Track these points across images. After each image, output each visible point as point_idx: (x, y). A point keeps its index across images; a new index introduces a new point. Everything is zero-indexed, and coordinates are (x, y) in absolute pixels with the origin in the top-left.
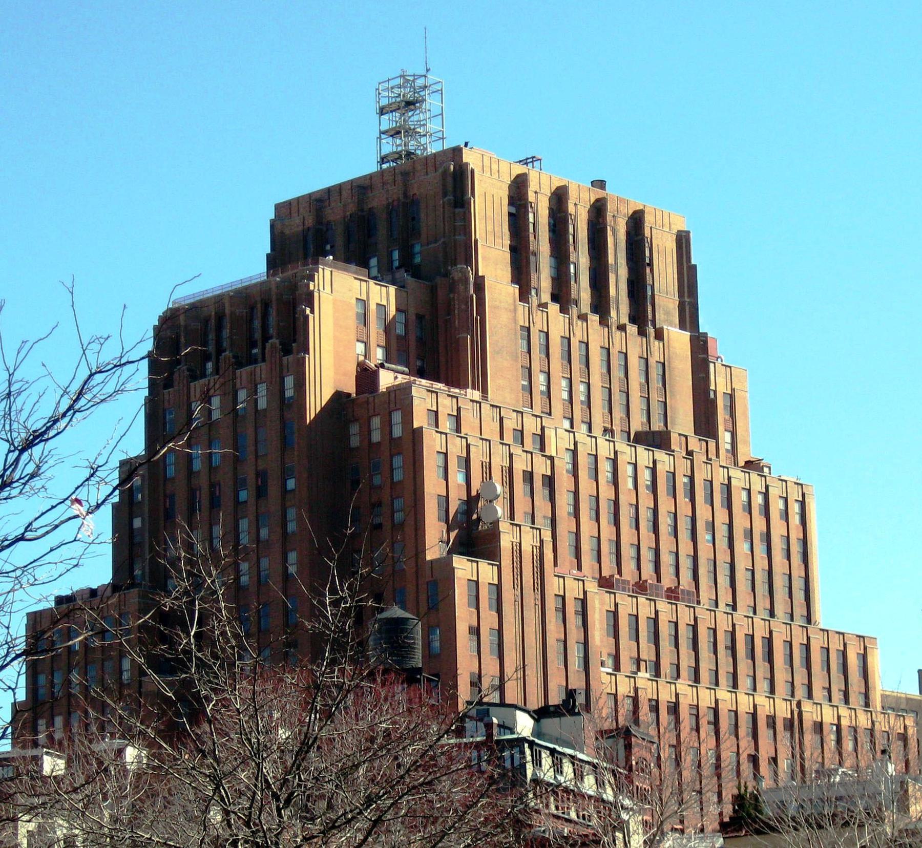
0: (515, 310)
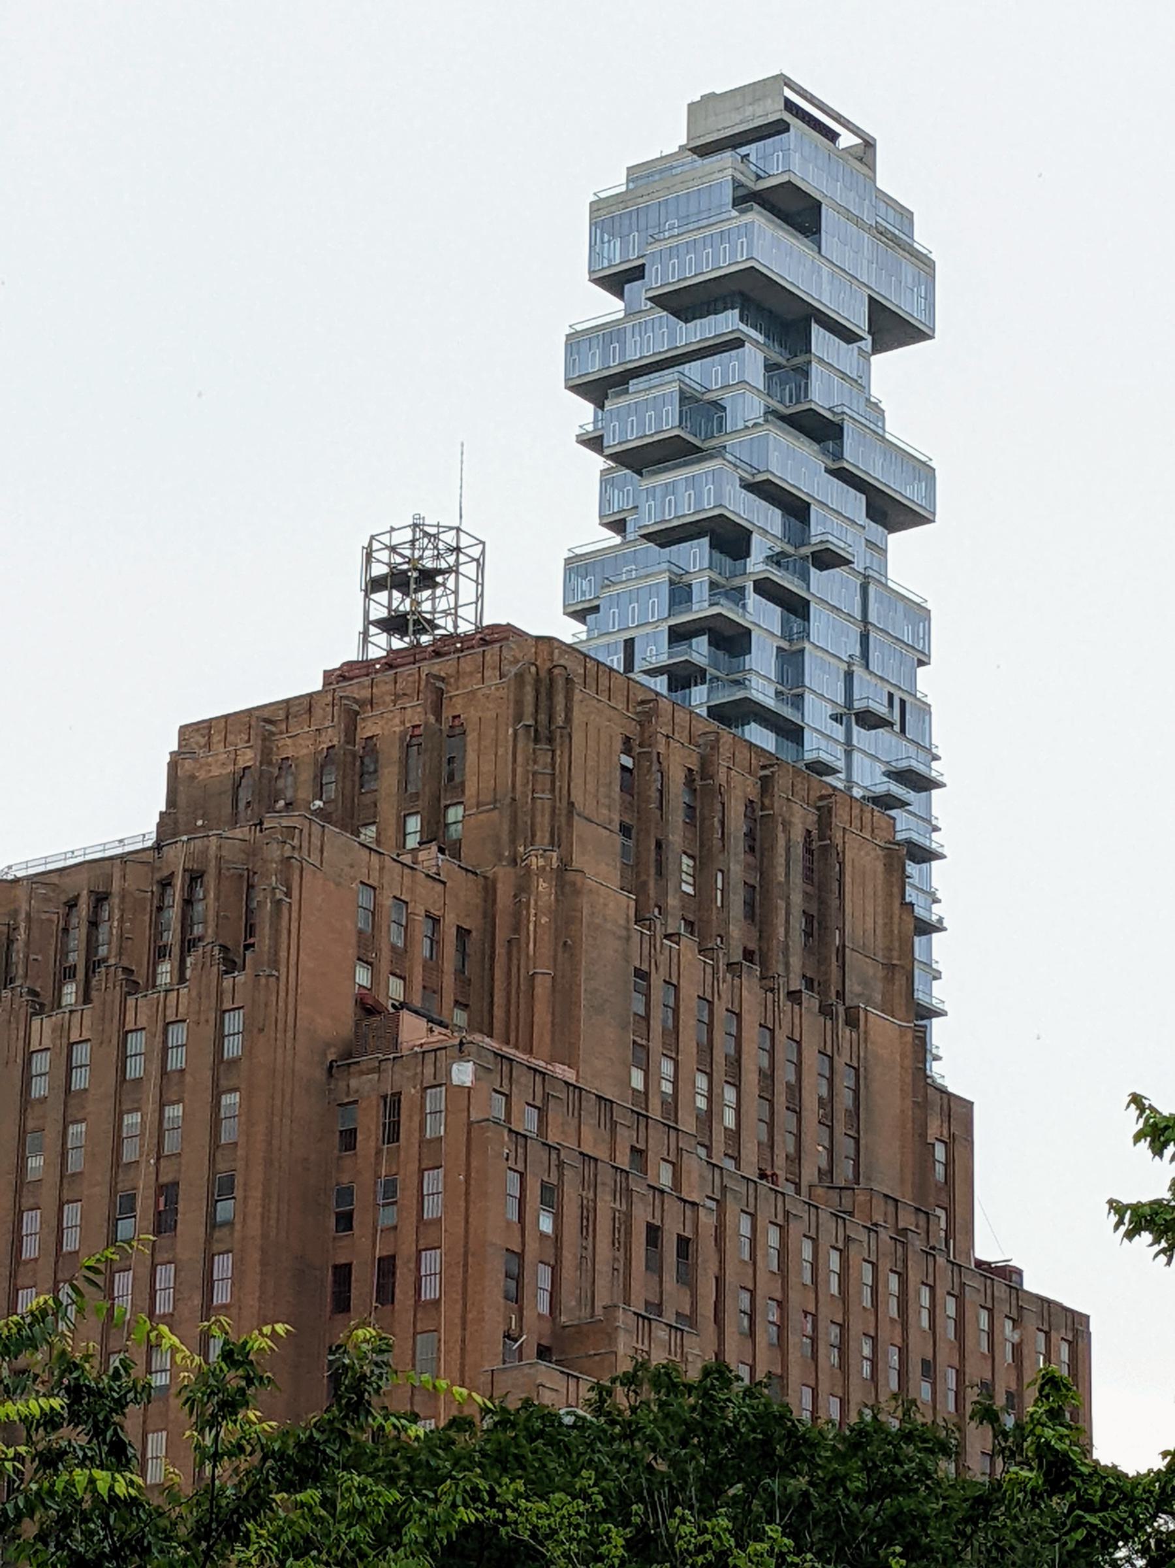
0: (628, 939)
